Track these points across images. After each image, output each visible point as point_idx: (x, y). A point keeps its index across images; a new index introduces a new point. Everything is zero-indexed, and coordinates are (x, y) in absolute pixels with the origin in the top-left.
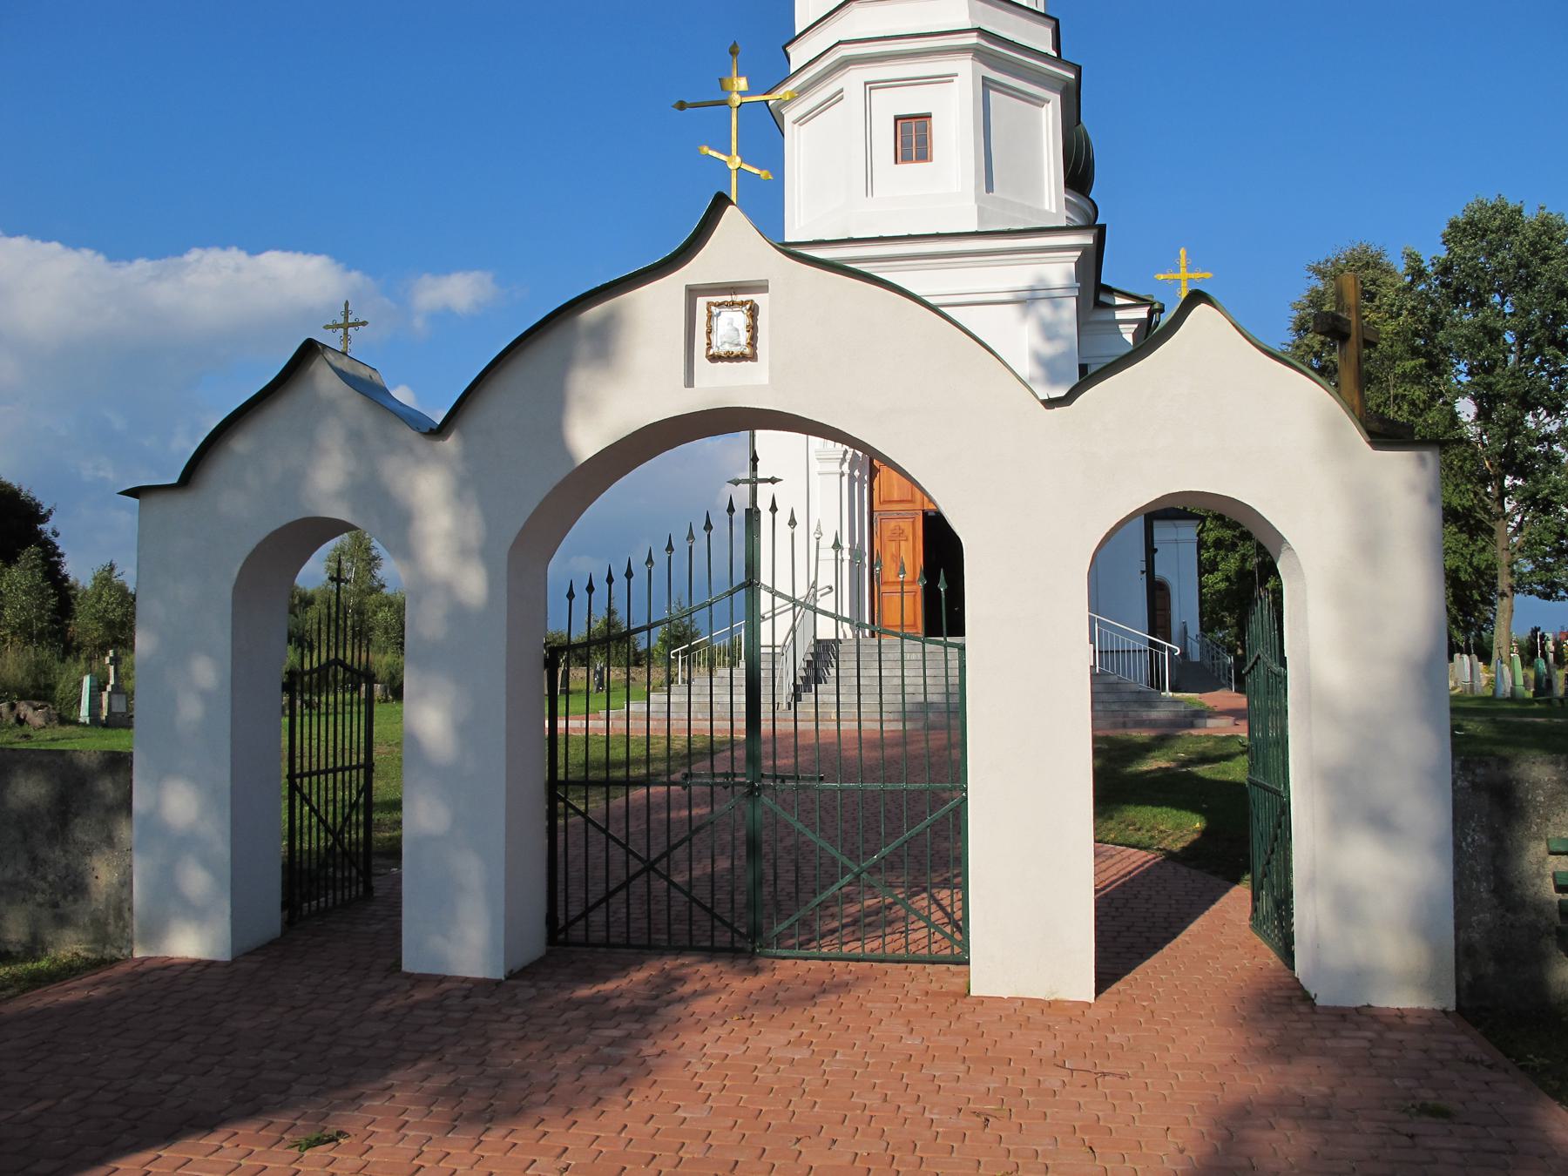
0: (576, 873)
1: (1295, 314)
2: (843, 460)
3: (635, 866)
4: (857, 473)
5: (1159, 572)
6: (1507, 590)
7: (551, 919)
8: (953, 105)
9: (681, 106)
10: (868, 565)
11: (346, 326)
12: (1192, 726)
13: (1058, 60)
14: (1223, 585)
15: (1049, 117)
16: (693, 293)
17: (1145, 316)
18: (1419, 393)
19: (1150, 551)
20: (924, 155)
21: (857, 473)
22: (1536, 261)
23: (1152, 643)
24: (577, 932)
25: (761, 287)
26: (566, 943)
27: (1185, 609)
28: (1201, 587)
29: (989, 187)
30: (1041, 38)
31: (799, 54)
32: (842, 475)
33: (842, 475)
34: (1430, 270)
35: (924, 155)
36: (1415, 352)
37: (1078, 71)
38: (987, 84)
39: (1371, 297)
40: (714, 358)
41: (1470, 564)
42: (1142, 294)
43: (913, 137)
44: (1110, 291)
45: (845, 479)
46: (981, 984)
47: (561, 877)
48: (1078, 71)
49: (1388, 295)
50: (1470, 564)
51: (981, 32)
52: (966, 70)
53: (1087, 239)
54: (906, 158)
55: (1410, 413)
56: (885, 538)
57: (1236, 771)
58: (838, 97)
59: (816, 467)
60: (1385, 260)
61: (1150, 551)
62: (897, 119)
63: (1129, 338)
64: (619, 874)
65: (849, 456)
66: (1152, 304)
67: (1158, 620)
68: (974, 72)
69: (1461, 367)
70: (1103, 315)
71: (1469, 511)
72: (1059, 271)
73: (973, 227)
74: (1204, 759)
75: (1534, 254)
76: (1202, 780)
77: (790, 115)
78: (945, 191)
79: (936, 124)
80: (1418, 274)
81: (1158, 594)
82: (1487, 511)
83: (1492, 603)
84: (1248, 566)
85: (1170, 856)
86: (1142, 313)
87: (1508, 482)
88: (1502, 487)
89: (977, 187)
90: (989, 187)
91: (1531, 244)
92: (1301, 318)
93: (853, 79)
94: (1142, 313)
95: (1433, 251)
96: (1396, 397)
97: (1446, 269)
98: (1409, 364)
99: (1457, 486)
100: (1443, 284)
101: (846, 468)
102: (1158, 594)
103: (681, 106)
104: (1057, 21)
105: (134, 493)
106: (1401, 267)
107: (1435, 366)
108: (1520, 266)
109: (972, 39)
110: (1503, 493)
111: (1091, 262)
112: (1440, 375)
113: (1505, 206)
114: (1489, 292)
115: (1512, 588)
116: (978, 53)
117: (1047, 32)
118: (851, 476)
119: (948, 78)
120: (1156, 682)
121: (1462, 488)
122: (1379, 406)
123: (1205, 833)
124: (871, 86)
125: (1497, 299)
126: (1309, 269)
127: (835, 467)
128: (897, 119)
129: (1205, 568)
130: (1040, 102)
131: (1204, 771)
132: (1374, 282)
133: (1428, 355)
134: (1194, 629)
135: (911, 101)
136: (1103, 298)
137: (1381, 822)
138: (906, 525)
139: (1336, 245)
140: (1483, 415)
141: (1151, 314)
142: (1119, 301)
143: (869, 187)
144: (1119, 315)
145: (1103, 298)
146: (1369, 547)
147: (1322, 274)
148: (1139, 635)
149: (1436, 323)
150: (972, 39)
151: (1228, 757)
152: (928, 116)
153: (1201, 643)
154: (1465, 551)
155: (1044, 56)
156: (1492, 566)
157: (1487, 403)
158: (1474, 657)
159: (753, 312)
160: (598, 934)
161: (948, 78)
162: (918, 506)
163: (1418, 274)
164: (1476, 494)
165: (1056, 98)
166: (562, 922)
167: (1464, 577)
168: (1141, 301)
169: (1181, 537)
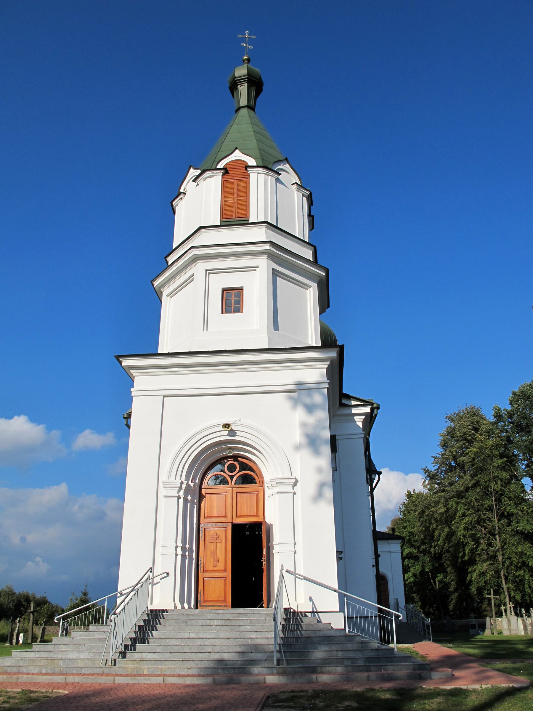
2: (180, 488)
4: (189, 497)
5: (381, 570)
8: (256, 283)
10: (194, 559)
13: (315, 262)
14: (412, 580)
15: (311, 294)
17: (369, 411)
18: (505, 475)
19: (377, 556)
20: (238, 309)
21: (189, 497)
23: (380, 610)
27: (397, 590)
28: (404, 580)
29: (276, 328)
30: (309, 254)
32: (179, 498)
33: (179, 498)
35: (238, 309)
36: (501, 456)
37: (327, 271)
38: (275, 273)
42: (366, 399)
43: (232, 301)
44: (349, 397)
45: (181, 501)
48: (327, 271)
49: (484, 428)
51: (272, 243)
52: (263, 264)
53: (333, 354)
54: (228, 311)
55: (502, 486)
56: (207, 539)
58: (190, 279)
59: (163, 492)
60: (482, 413)
61: (377, 556)
62: (224, 290)
63: (360, 424)
65: (184, 486)
66: (372, 404)
67: (382, 596)
70: (345, 411)
72: (316, 373)
77: (165, 293)
78: (251, 327)
79: (246, 294)
80: (498, 416)
81: (381, 582)
84: (427, 569)
90: (276, 328)
92: (444, 440)
93: (200, 267)
95: (506, 406)
96: (494, 478)
97: (511, 416)
98: (500, 461)
101: (182, 493)
102: (381, 582)
109: (267, 247)
111: (336, 372)
116: (271, 256)
118: (186, 501)
119: (253, 268)
120: (386, 638)
122: (486, 482)
124: (209, 272)
126: (447, 417)
127: (175, 493)
128: (224, 290)
129: (406, 570)
130: (306, 287)
132: (478, 422)
135: (232, 281)
136: (344, 401)
138: (221, 532)
139: (458, 407)
141: (372, 410)
142: (354, 403)
143: (205, 326)
144: (354, 411)
145: (344, 401)
147: (452, 420)
148: (372, 605)
150: (267, 247)
152: (241, 289)
161: (253, 268)
162: (229, 519)
165: (315, 286)
168: (366, 403)
169: (392, 550)
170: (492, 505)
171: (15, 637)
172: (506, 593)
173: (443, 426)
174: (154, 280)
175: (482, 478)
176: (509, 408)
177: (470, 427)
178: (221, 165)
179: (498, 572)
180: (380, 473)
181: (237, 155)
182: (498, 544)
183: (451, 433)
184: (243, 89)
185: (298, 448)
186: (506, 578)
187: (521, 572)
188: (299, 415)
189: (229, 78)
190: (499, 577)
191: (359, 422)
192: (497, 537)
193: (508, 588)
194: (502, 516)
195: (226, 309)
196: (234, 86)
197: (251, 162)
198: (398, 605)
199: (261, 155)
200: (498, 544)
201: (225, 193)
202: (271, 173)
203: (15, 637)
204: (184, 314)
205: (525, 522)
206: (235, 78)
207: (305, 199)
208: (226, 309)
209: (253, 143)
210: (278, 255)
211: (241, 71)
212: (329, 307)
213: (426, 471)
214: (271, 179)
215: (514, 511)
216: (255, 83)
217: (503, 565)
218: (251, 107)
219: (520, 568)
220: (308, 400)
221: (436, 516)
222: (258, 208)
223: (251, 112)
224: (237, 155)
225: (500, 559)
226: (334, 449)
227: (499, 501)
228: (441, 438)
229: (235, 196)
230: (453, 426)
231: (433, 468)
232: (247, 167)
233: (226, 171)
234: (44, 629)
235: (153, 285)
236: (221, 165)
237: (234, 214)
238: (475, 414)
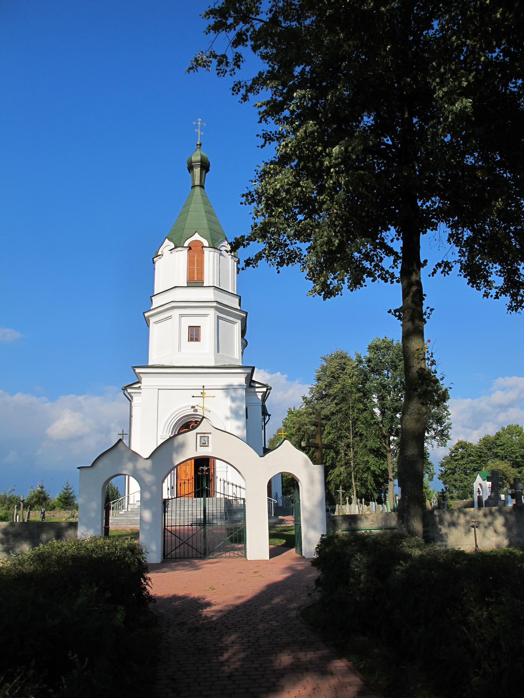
0: (169, 543)
1: (316, 374)
3: (181, 542)
6: (392, 478)
7: (164, 554)
8: (207, 324)
9: (193, 397)
11: (123, 434)
12: (281, 524)
13: (240, 311)
15: (237, 327)
16: (197, 434)
17: (265, 390)
22: (397, 361)
24: (169, 556)
25: (210, 433)
26: (167, 558)
29: (218, 352)
30: (234, 303)
31: (157, 302)
34: (364, 360)
35: (197, 340)
36: (359, 390)
38: (219, 318)
39: (344, 369)
40: (201, 446)
41: (379, 469)
43: (194, 334)
46: (249, 558)
47: (166, 544)
50: (379, 469)
51: (217, 302)
52: (212, 313)
57: (293, 533)
58: (170, 317)
62: (189, 327)
63: (260, 397)
64: (178, 545)
66: (268, 387)
68: (215, 314)
69: (374, 396)
70: (252, 390)
71: (379, 449)
72: (241, 380)
73: (213, 365)
74: (285, 531)
75: (396, 358)
76: (285, 534)
77: (152, 320)
78: (204, 352)
79: (202, 330)
82: (385, 448)
83: (388, 483)
85: (278, 546)
86: (264, 390)
87: (392, 438)
88: (389, 440)
89: (214, 351)
90: (218, 352)
91: (397, 355)
93: (176, 313)
94: (264, 390)
97: (369, 361)
99: (374, 440)
100: (369, 366)
103: (193, 397)
104: (240, 297)
105: (79, 468)
106: (354, 358)
107: (366, 394)
108: (392, 362)
109: (215, 304)
110: (390, 443)
112: (368, 398)
113: (451, 236)
114: (383, 370)
115: (394, 477)
116: (216, 308)
117: (237, 300)
119: (206, 315)
121: (376, 440)
123: (286, 543)
124: (181, 315)
125: (386, 372)
128: (189, 327)
130: (235, 323)
131: (286, 533)
132: (344, 364)
133: (363, 392)
134: (280, 495)
135: (194, 322)
136: (252, 384)
137: (314, 528)
139: (331, 349)
140: (383, 413)
141: (267, 390)
142: (257, 385)
144: (257, 390)
145: (252, 384)
146: (312, 482)
149: (366, 379)
150: (215, 304)
151: (292, 530)
152: (200, 327)
153: (282, 500)
154: (377, 464)
155: (236, 309)
156: (386, 470)
157: (383, 409)
158: (376, 503)
159: (208, 438)
160: (173, 556)
161: (206, 315)
163: (360, 362)
164: (381, 443)
165: (239, 322)
166: (166, 554)
167: (377, 473)
170: (350, 426)
171: (15, 518)
172: (354, 488)
173: (319, 364)
174: (145, 312)
175: (344, 406)
176: (368, 355)
177: (338, 367)
178: (186, 244)
179: (350, 474)
180: (269, 415)
181: (197, 237)
182: (351, 454)
183: (324, 369)
184: (197, 171)
185: (227, 418)
186: (355, 479)
187: (365, 475)
188: (228, 403)
189: (186, 159)
190: (351, 478)
191: (260, 396)
192: (351, 449)
193: (356, 485)
194: (356, 434)
195: (191, 339)
196: (191, 168)
197: (206, 243)
198: (277, 494)
199: (211, 235)
200: (351, 454)
201: (190, 263)
202: (217, 251)
203: (15, 518)
204: (164, 340)
205: (372, 441)
206: (192, 163)
207: (235, 263)
208: (191, 339)
209: (207, 232)
210: (221, 308)
211: (196, 158)
212: (270, 483)
213: (304, 398)
214: (217, 254)
215: (364, 432)
216: (205, 166)
217: (354, 469)
218: (202, 186)
219: (365, 472)
220: (234, 394)
221: (309, 432)
222: (209, 277)
223: (202, 189)
224: (197, 237)
225: (352, 464)
226: (247, 417)
227: (354, 423)
228: (316, 374)
229: (196, 265)
230: (325, 364)
231: (309, 396)
232: (203, 247)
233: (190, 248)
234: (29, 513)
235: (144, 315)
236: (186, 244)
237: (195, 281)
238: (343, 357)
